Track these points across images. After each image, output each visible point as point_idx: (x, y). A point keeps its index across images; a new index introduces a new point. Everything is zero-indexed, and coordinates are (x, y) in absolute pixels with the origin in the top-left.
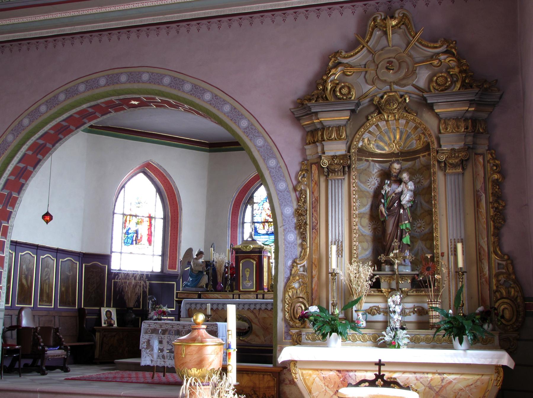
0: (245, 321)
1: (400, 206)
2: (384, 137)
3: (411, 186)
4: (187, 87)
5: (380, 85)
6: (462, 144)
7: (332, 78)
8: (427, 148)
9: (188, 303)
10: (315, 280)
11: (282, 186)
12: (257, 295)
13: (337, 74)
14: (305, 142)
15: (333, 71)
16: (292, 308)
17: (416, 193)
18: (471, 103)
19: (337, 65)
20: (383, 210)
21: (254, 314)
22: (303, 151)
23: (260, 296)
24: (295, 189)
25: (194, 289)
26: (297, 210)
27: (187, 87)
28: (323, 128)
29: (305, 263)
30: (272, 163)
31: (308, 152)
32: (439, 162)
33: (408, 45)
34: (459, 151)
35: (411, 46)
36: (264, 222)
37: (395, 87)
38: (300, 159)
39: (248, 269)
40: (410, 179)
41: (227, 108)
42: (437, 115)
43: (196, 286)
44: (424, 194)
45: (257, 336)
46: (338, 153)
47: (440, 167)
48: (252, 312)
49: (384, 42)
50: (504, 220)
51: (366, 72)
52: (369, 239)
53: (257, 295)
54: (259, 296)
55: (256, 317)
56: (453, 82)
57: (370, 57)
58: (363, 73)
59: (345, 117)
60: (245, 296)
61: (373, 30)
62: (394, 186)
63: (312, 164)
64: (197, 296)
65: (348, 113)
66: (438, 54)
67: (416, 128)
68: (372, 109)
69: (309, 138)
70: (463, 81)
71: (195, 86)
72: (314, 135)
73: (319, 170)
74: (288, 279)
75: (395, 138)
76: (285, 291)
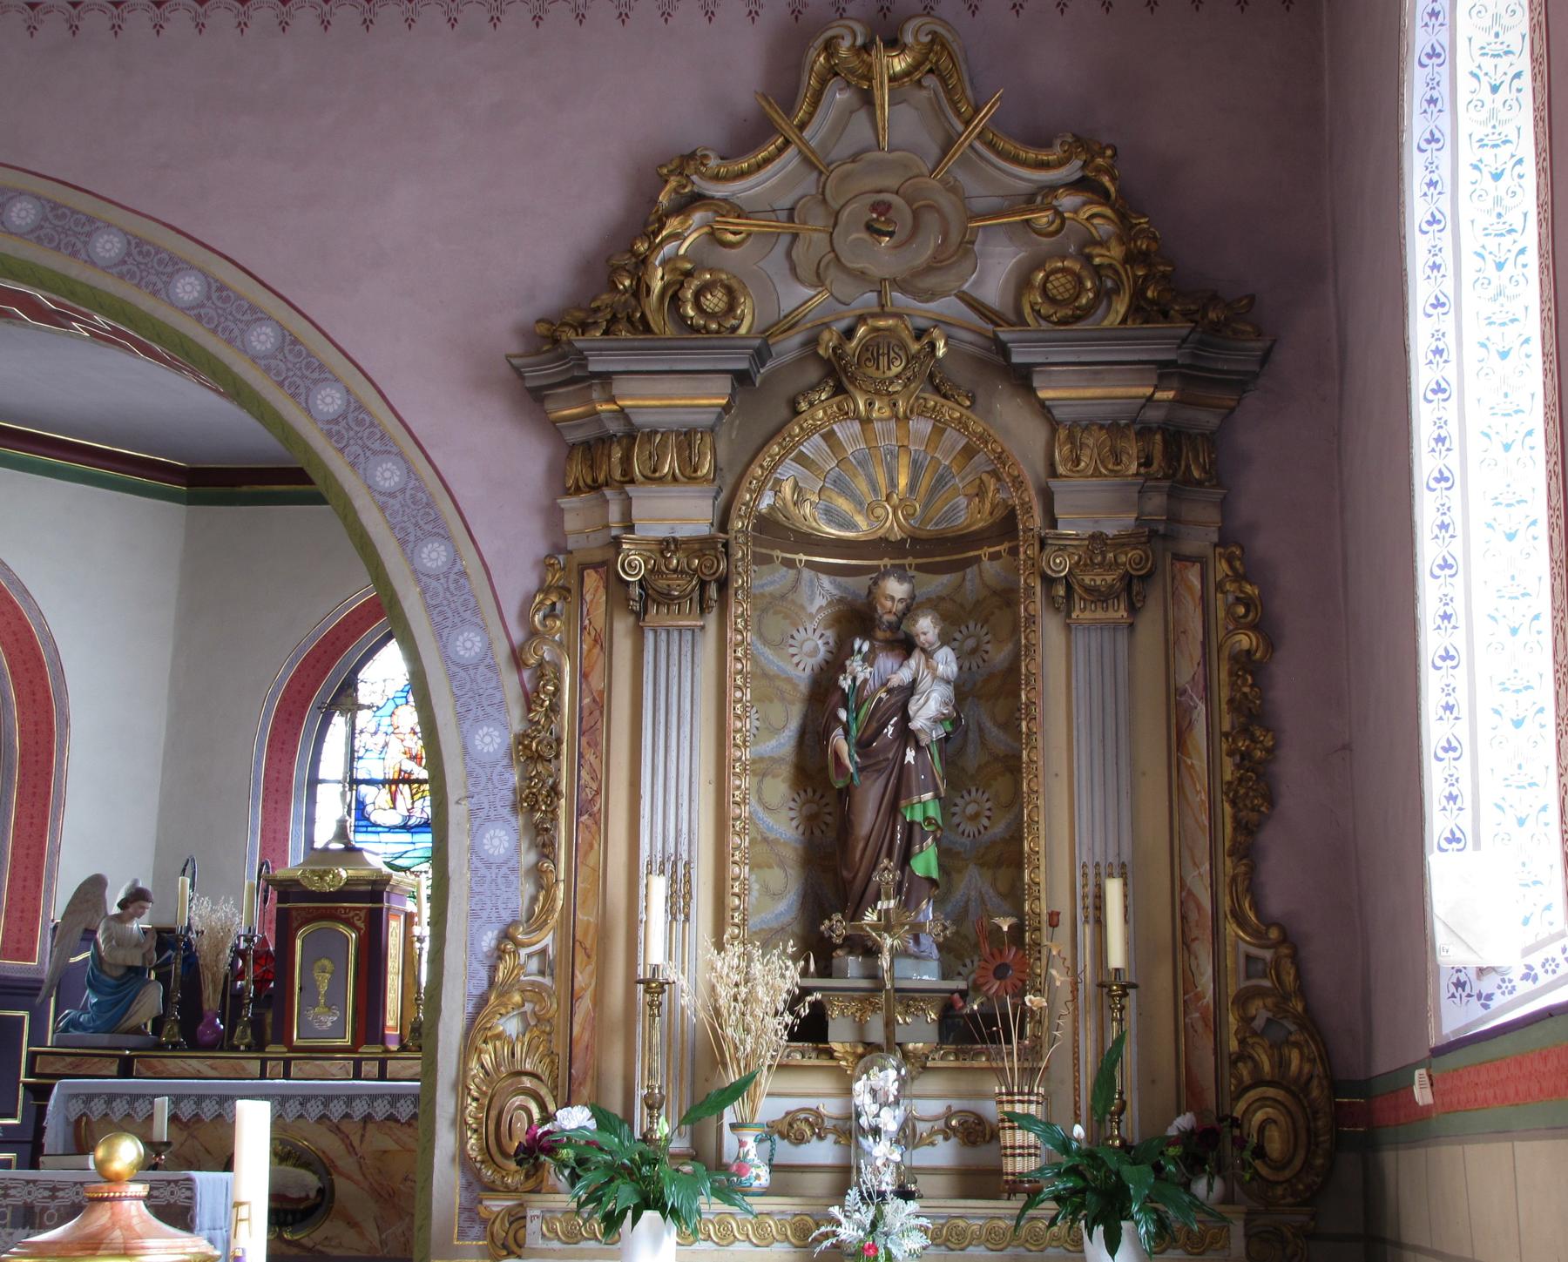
0: (306, 1165)
1: (907, 735)
2: (853, 479)
3: (946, 662)
4: (108, 246)
5: (841, 285)
6: (1129, 519)
7: (668, 249)
8: (1006, 526)
9: (76, 1096)
10: (584, 1006)
11: (468, 644)
12: (358, 1064)
13: (685, 237)
14: (561, 485)
15: (673, 225)
16: (493, 1113)
17: (963, 691)
18: (1164, 371)
19: (689, 202)
20: (844, 748)
21: (345, 1138)
22: (553, 516)
23: (370, 1068)
24: (517, 659)
25: (104, 1039)
26: (521, 740)
27: (108, 246)
28: (631, 436)
29: (547, 940)
30: (434, 556)
31: (571, 523)
32: (1049, 582)
33: (947, 146)
34: (1120, 542)
35: (956, 153)
36: (396, 782)
37: (898, 298)
38: (540, 548)
39: (326, 962)
40: (945, 639)
41: (263, 339)
42: (1044, 409)
43: (111, 1027)
44: (993, 692)
45: (352, 1223)
46: (684, 531)
47: (1050, 599)
48: (337, 1129)
49: (860, 128)
50: (1271, 799)
51: (795, 236)
52: (791, 854)
53: (358, 1064)
54: (365, 1067)
55: (351, 1148)
56: (1104, 295)
57: (809, 183)
58: (784, 241)
59: (711, 396)
60: (309, 1067)
61: (823, 83)
62: (885, 662)
63: (583, 567)
64: (114, 1069)
65: (724, 384)
66: (1052, 189)
67: (969, 452)
68: (813, 373)
69: (577, 471)
70: (1138, 294)
71: (137, 245)
72: (598, 461)
73: (609, 591)
74: (482, 1001)
75: (893, 484)
76: (469, 1047)
